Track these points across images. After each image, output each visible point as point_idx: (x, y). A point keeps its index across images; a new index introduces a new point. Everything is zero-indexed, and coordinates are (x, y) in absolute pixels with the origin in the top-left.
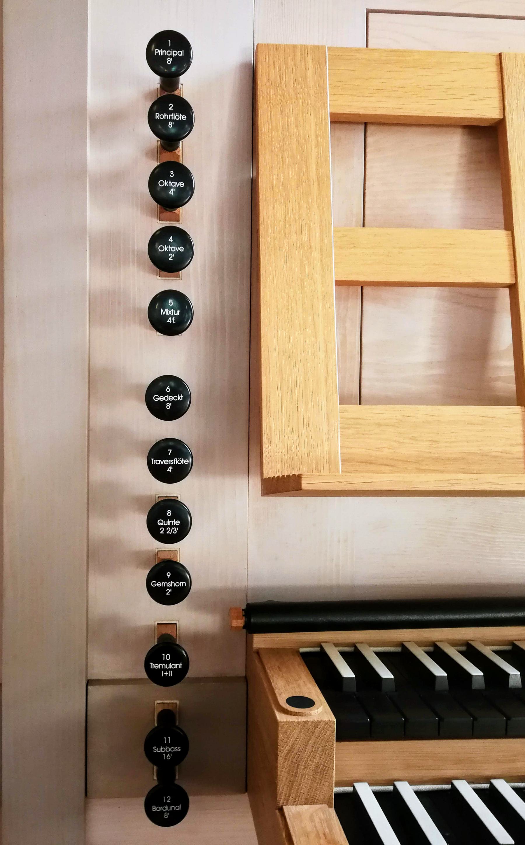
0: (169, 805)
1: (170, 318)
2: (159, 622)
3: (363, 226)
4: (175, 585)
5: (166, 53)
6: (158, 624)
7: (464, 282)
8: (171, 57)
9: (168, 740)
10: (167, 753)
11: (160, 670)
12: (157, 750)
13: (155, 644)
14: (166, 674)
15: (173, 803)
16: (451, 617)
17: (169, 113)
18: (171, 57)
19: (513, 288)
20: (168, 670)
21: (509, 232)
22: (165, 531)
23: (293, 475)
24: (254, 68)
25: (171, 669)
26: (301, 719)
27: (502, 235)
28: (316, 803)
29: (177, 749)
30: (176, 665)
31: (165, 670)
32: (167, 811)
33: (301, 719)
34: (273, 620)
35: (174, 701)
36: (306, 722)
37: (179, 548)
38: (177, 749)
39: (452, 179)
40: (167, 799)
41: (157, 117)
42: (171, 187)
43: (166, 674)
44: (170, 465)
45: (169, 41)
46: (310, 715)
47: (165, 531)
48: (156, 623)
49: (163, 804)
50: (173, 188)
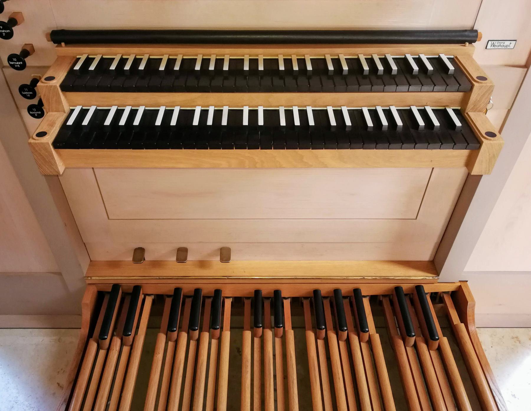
3: (467, 281)
6: (25, 44)
7: (414, 112)
9: (26, 90)
10: (28, 94)
12: (23, 93)
14: (17, 66)
16: (246, 36)
20: (17, 65)
24: (370, 344)
26: (46, 85)
30: (20, 63)
31: (16, 65)
33: (46, 85)
34: (242, 36)
35: (39, 75)
36: (47, 86)
37: (489, 41)
46: (49, 83)
48: (24, 43)
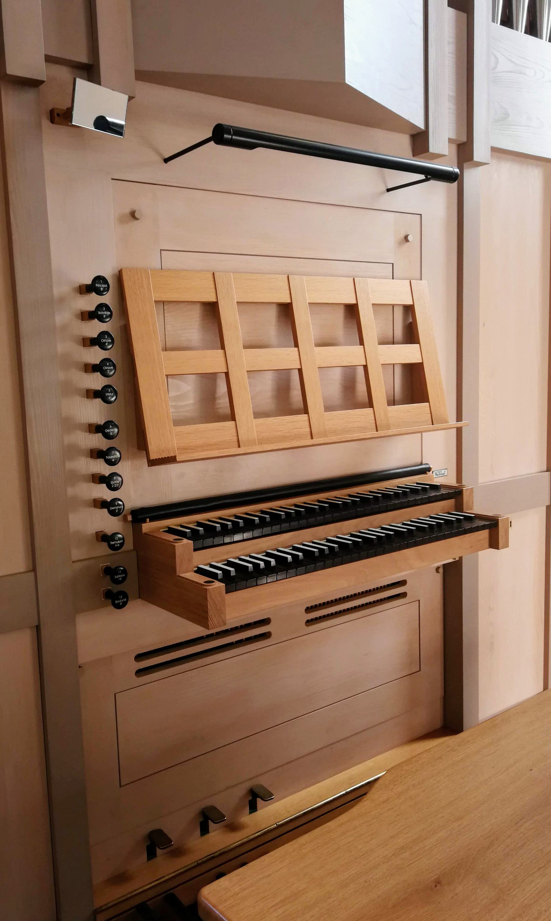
0: (122, 599)
1: (110, 397)
2: (96, 531)
4: (119, 508)
5: (100, 286)
8: (102, 287)
9: (120, 572)
10: (120, 578)
11: (114, 544)
12: (116, 577)
13: (428, 407)
15: (123, 598)
17: (104, 311)
18: (102, 287)
19: (227, 374)
20: (117, 544)
21: (224, 350)
22: (114, 486)
23: (167, 457)
25: (118, 543)
26: (182, 543)
27: (221, 352)
28: (189, 572)
29: (124, 575)
30: (120, 541)
32: (121, 602)
35: (108, 564)
38: (124, 575)
39: (198, 323)
40: (121, 597)
41: (99, 313)
42: (106, 342)
43: (117, 545)
44: (113, 458)
45: (101, 281)
47: (114, 486)
49: (119, 599)
50: (107, 342)
